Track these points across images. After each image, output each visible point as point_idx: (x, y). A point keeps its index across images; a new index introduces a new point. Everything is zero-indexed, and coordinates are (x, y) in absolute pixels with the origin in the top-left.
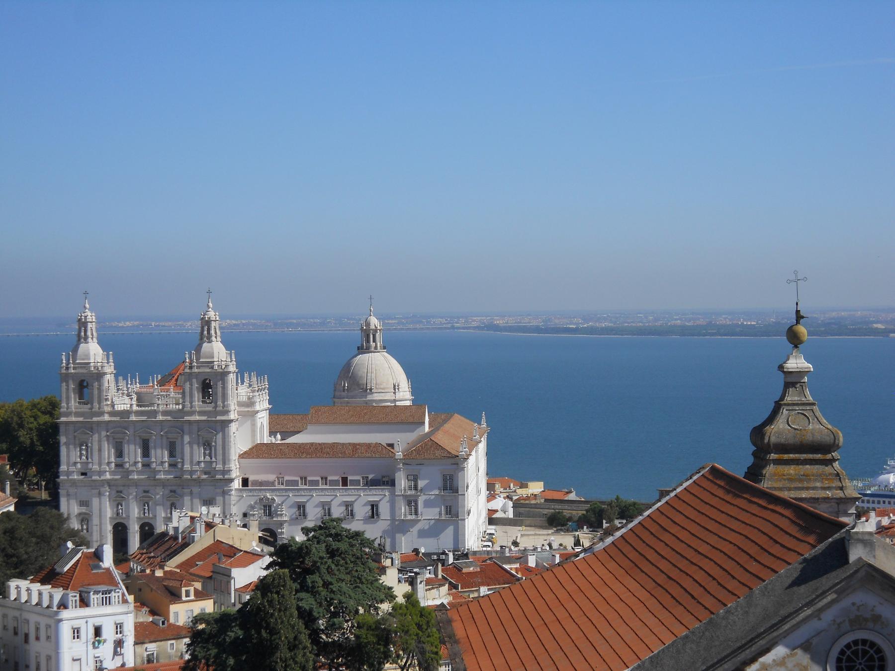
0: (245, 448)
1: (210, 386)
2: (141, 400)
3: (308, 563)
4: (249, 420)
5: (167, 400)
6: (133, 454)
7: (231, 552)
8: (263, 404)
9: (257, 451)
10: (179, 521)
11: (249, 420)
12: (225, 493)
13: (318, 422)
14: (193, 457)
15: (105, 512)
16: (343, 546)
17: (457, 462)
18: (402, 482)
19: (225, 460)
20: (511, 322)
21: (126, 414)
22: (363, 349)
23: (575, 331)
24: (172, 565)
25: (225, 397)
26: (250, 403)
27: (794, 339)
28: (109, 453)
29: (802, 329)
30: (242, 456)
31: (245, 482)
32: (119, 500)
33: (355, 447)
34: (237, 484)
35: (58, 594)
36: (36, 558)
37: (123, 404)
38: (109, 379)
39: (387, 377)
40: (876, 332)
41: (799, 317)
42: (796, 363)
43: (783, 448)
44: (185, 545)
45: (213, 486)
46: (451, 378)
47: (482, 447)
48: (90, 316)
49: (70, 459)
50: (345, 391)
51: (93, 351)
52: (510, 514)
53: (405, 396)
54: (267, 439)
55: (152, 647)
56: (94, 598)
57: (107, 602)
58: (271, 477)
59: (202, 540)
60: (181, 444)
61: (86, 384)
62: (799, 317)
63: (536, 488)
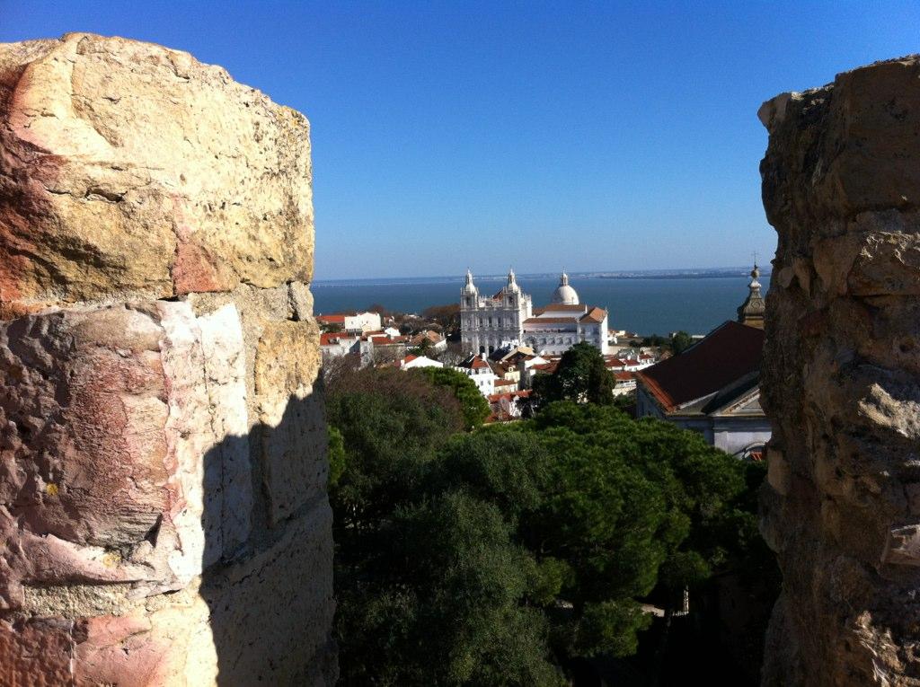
0: (524, 320)
1: (512, 298)
2: (487, 303)
3: (577, 356)
4: (525, 310)
5: (496, 304)
6: (486, 322)
7: (524, 355)
8: (529, 305)
9: (528, 321)
10: (505, 344)
11: (525, 310)
12: (518, 336)
13: (548, 310)
14: (507, 323)
15: (477, 343)
16: (588, 352)
17: (599, 323)
18: (580, 331)
19: (518, 324)
20: (617, 275)
21: (483, 308)
22: (562, 285)
23: (632, 278)
24: (504, 359)
25: (517, 302)
26: (525, 304)
27: (754, 274)
28: (477, 322)
29: (758, 273)
30: (524, 322)
31: (525, 331)
32: (482, 339)
33: (562, 319)
34: (522, 332)
35: (468, 370)
36: (872, 325)
37: (482, 305)
38: (519, 295)
39: (571, 296)
40: (743, 276)
41: (756, 267)
42: (755, 284)
43: (751, 315)
44: (507, 353)
45: (514, 333)
46: (594, 293)
47: (606, 319)
48: (512, 274)
49: (464, 324)
50: (556, 300)
51: (472, 288)
52: (616, 342)
53: (576, 302)
54: (531, 317)
55: (500, 388)
56: (480, 371)
57: (484, 372)
58: (542, 329)
59: (513, 352)
60: (503, 320)
61: (469, 298)
62: (756, 267)
63: (622, 333)
